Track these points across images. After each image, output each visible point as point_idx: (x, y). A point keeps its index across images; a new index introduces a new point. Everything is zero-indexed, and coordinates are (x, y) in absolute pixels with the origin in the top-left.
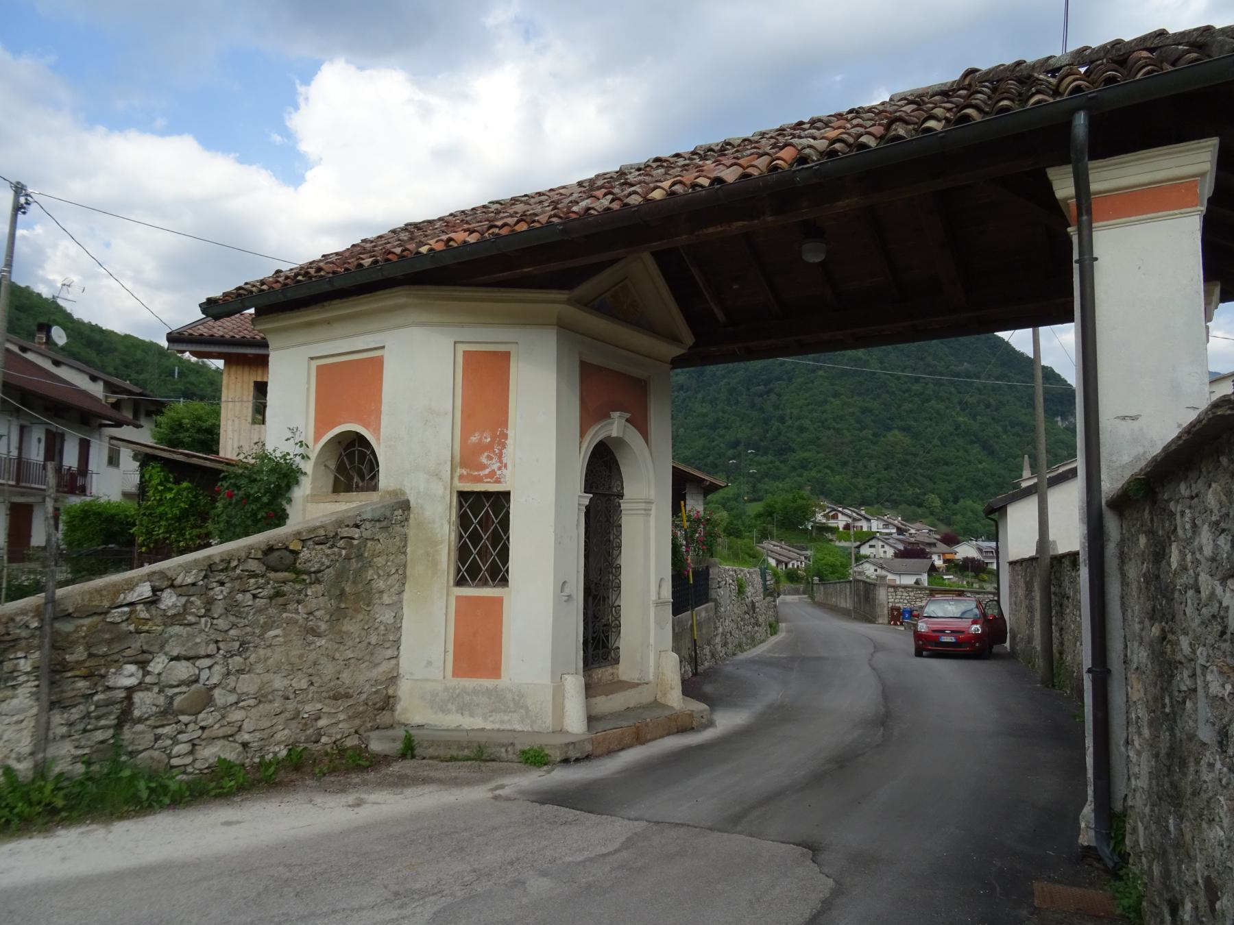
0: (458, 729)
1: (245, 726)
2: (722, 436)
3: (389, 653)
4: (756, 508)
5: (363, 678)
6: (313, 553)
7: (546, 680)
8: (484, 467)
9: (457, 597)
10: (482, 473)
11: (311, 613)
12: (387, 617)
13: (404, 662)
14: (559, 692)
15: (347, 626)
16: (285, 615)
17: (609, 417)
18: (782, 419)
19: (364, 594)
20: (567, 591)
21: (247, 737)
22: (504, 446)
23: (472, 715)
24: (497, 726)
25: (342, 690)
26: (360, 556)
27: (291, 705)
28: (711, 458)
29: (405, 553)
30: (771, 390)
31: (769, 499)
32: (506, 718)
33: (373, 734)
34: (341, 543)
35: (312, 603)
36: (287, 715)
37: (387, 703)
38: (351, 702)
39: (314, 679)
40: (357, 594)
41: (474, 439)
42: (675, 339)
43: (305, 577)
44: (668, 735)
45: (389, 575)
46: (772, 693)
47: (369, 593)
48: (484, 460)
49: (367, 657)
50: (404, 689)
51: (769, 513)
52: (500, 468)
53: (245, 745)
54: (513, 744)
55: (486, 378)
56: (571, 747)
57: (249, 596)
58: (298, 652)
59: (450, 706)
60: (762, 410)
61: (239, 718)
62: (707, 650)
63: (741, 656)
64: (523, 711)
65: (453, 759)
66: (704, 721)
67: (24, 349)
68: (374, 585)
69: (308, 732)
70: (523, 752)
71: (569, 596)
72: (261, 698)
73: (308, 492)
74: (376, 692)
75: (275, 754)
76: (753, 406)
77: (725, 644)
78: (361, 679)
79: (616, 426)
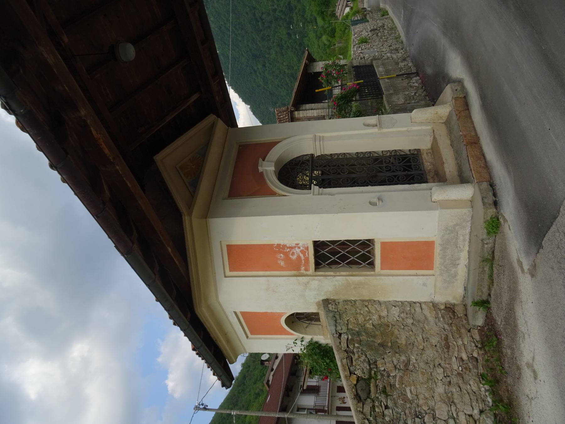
0: (468, 267)
1: (469, 413)
2: (286, 42)
3: (418, 310)
4: (320, 21)
5: (434, 326)
6: (358, 367)
7: (436, 214)
8: (299, 257)
9: (382, 269)
10: (303, 258)
11: (395, 366)
12: (395, 312)
13: (423, 300)
14: (444, 205)
15: (402, 340)
16: (397, 386)
17: (262, 173)
18: (275, 10)
19: (382, 329)
20: (375, 200)
21: (476, 412)
22: (285, 246)
23: (459, 259)
24: (467, 243)
25: (443, 343)
26: (358, 334)
27: (454, 380)
28: (297, 47)
29: (355, 301)
30: (260, 17)
31: (315, 14)
32: (461, 238)
33: (472, 322)
34: (351, 347)
35: (389, 366)
36: (460, 382)
37: (450, 309)
38: (450, 336)
39: (437, 363)
40: (383, 334)
41: (282, 263)
42: (212, 127)
43: (373, 372)
44: (470, 117)
45: (369, 312)
46: (433, 29)
47: (381, 325)
48: (294, 257)
49: (421, 325)
50: (441, 299)
51: (322, 13)
52: (299, 248)
53: (481, 412)
54: (482, 240)
55: (244, 258)
56: (486, 200)
57: (386, 412)
58: (420, 376)
59: (452, 272)
60: (271, 22)
61: (464, 417)
62: (402, 64)
63: (403, 38)
64: (457, 227)
65: (491, 277)
66: (459, 88)
67: (272, 370)
68: (376, 323)
69: (471, 367)
70: (489, 233)
71: (379, 199)
72: (451, 402)
73: (322, 337)
74: (444, 318)
75: (486, 391)
76: (269, 27)
77: (397, 50)
78: (436, 329)
79: (268, 168)
